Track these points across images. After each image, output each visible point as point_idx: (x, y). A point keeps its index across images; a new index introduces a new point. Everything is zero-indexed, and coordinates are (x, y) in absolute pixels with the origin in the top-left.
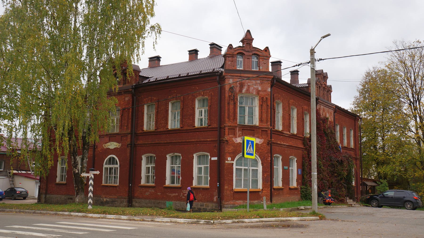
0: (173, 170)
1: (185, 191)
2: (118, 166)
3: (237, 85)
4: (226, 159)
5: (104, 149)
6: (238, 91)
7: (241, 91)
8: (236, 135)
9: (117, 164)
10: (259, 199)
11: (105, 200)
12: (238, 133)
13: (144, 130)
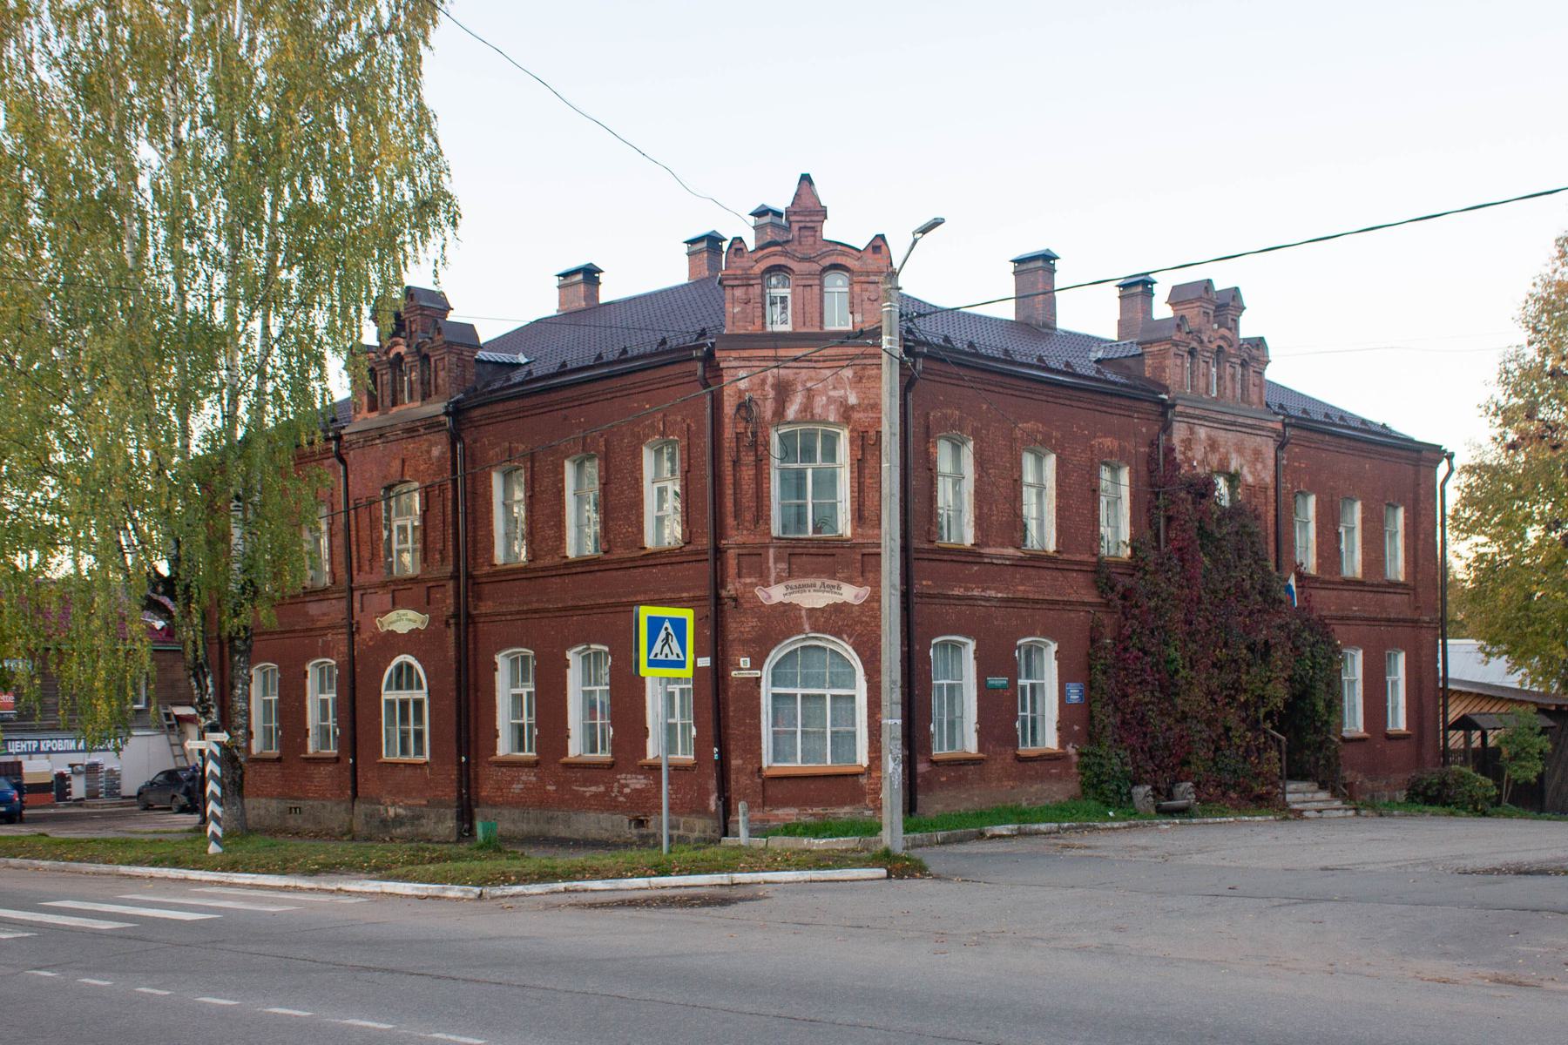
0: (591, 709)
1: (623, 776)
2: (422, 694)
5: (379, 634)
6: (768, 414)
7: (779, 413)
8: (768, 577)
9: (420, 687)
10: (859, 802)
11: (391, 812)
13: (496, 562)
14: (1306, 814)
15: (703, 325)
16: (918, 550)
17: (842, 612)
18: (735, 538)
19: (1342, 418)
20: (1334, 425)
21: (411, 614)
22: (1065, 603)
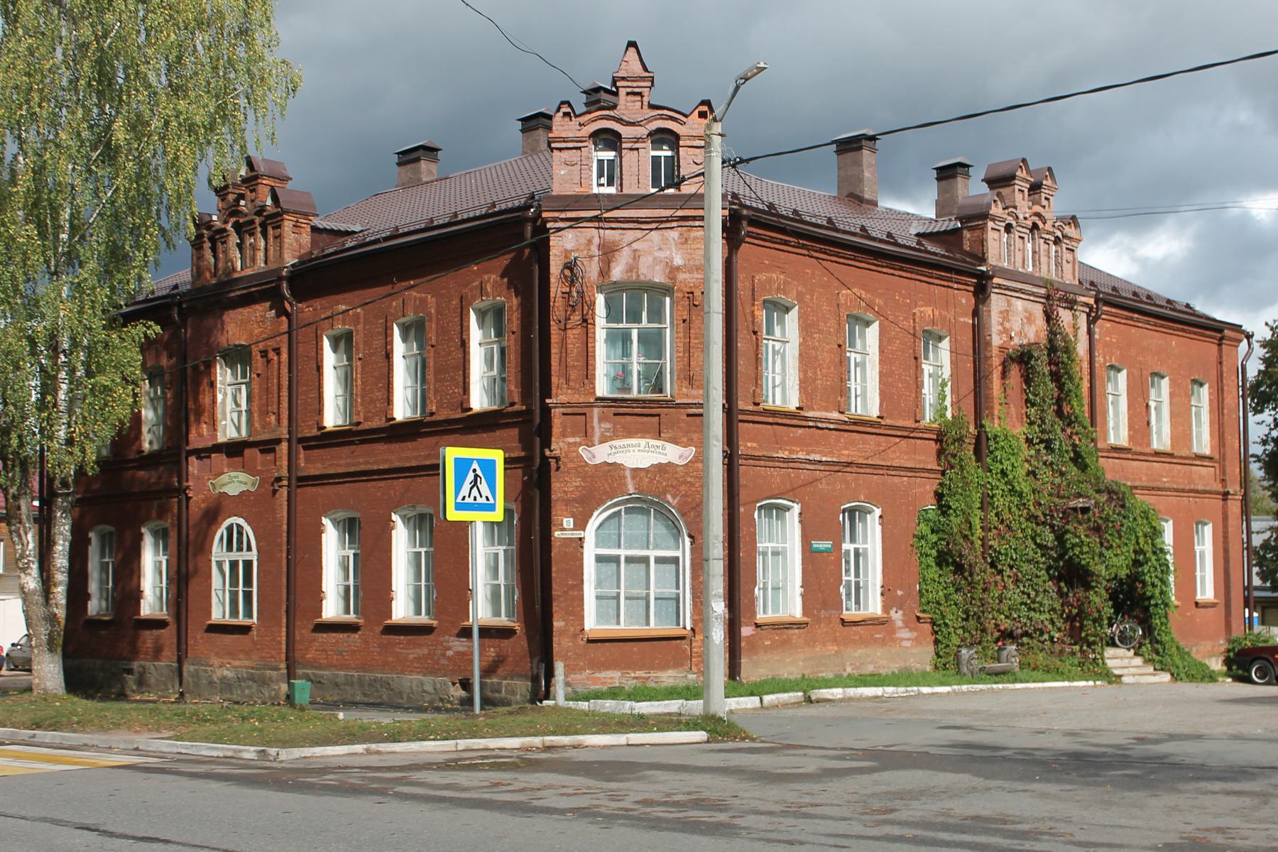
2: (253, 556)
3: (590, 253)
4: (555, 525)
8: (592, 436)
12: (600, 427)
14: (1124, 679)
15: (532, 190)
16: (743, 412)
17: (666, 472)
18: (561, 396)
19: (1149, 297)
20: (1142, 302)
21: (243, 476)
22: (889, 468)
